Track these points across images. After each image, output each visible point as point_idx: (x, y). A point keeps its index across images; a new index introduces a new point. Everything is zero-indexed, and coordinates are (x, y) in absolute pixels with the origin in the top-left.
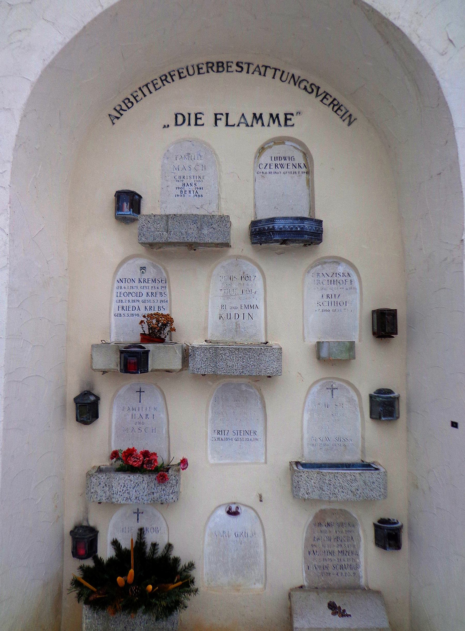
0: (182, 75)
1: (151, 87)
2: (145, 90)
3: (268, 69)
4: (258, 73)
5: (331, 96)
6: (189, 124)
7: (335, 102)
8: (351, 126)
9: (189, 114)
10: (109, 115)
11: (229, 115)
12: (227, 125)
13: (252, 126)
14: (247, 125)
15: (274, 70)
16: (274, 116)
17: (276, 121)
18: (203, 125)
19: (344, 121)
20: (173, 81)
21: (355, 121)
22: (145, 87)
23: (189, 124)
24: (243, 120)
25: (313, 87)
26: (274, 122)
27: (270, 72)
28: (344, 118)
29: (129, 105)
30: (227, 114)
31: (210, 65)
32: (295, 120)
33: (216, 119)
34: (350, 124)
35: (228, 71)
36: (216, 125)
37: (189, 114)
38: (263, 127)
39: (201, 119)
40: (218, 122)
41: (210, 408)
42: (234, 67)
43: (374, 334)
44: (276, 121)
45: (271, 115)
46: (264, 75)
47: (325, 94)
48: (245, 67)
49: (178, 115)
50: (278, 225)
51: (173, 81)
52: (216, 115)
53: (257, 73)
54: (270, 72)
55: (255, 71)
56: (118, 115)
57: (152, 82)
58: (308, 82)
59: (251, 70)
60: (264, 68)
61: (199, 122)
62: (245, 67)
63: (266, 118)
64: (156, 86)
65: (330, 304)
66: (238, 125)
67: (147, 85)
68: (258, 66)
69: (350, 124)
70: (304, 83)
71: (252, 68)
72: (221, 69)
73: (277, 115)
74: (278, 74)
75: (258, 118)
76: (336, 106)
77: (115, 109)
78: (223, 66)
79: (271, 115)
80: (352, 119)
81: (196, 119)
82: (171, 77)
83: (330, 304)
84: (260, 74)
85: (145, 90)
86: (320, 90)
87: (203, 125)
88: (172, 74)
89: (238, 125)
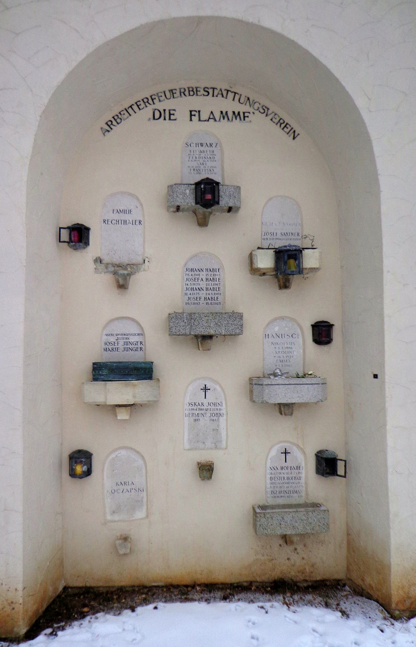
0: (161, 99)
1: (135, 107)
3: (229, 92)
4: (221, 95)
5: (139, 101)
6: (165, 119)
7: (281, 121)
8: (296, 139)
9: (164, 110)
10: (101, 128)
14: (215, 120)
15: (233, 94)
16: (236, 113)
17: (238, 117)
18: (175, 120)
19: (290, 136)
20: (154, 103)
21: (299, 136)
22: (130, 109)
23: (165, 119)
24: (212, 117)
27: (231, 95)
33: (191, 115)
34: (294, 138)
35: (197, 95)
36: (191, 120)
39: (174, 114)
41: (199, 343)
42: (202, 92)
43: (70, 475)
44: (238, 117)
45: (234, 113)
46: (226, 98)
48: (211, 91)
51: (154, 103)
52: (191, 111)
53: (220, 96)
54: (231, 95)
55: (218, 94)
56: (109, 129)
57: (136, 103)
58: (260, 104)
59: (216, 93)
60: (226, 91)
61: (172, 117)
62: (211, 91)
63: (230, 114)
64: (140, 107)
67: (131, 107)
68: (221, 90)
69: (294, 138)
71: (216, 92)
74: (237, 97)
75: (224, 115)
76: (283, 124)
77: (107, 123)
78: (193, 91)
79: (234, 113)
80: (296, 134)
81: (170, 114)
82: (152, 100)
83: (267, 337)
84: (223, 96)
85: (130, 110)
86: (269, 111)
87: (175, 120)
89: (208, 121)
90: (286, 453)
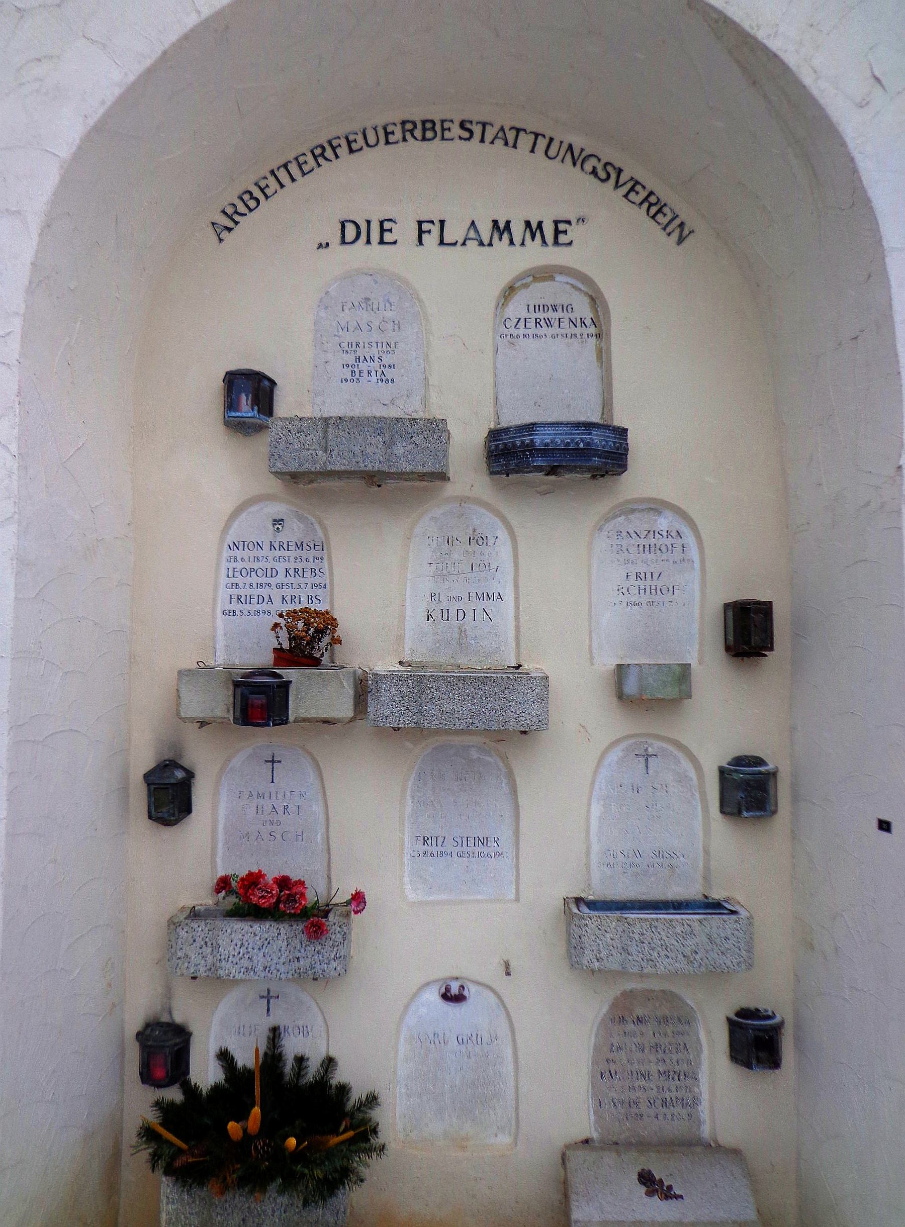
0: (354, 146)
1: (294, 169)
2: (282, 175)
3: (522, 134)
4: (502, 142)
5: (644, 187)
6: (368, 242)
7: (653, 199)
8: (684, 244)
9: (369, 222)
10: (213, 224)
11: (446, 224)
12: (442, 243)
13: (490, 244)
14: (481, 244)
15: (533, 137)
16: (534, 225)
17: (538, 235)
18: (395, 243)
19: (669, 234)
20: (337, 157)
21: (691, 235)
22: (282, 169)
23: (368, 242)
24: (472, 234)
25: (609, 168)
26: (533, 238)
27: (525, 141)
28: (669, 229)
29: (252, 204)
30: (442, 222)
31: (409, 126)
32: (573, 233)
33: (421, 232)
34: (680, 241)
35: (443, 138)
36: (420, 242)
37: (369, 222)
38: (512, 248)
39: (390, 230)
40: (425, 237)
42: (456, 131)
43: (728, 649)
44: (538, 235)
45: (528, 224)
46: (515, 146)
47: (632, 183)
48: (477, 130)
49: (347, 224)
50: (541, 438)
51: (337, 157)
52: (420, 223)
53: (499, 143)
54: (525, 141)
55: (496, 137)
56: (230, 224)
57: (296, 159)
58: (599, 160)
59: (489, 137)
60: (514, 132)
61: (388, 237)
62: (477, 130)
63: (518, 230)
64: (304, 167)
65: (642, 592)
66: (464, 244)
67: (285, 166)
68: (502, 129)
69: (680, 241)
70: (592, 162)
71: (490, 133)
72: (429, 134)
73: (540, 224)
74: (542, 143)
75: (502, 229)
76: (654, 206)
77: (224, 212)
78: (433, 129)
79: (528, 224)
80: (686, 232)
81: (382, 230)
82: (334, 149)
83: (642, 592)
84: (506, 144)
85: (282, 175)
86: (622, 175)
87: (395, 243)
88: (335, 143)
89: (464, 244)
90: (273, 762)
